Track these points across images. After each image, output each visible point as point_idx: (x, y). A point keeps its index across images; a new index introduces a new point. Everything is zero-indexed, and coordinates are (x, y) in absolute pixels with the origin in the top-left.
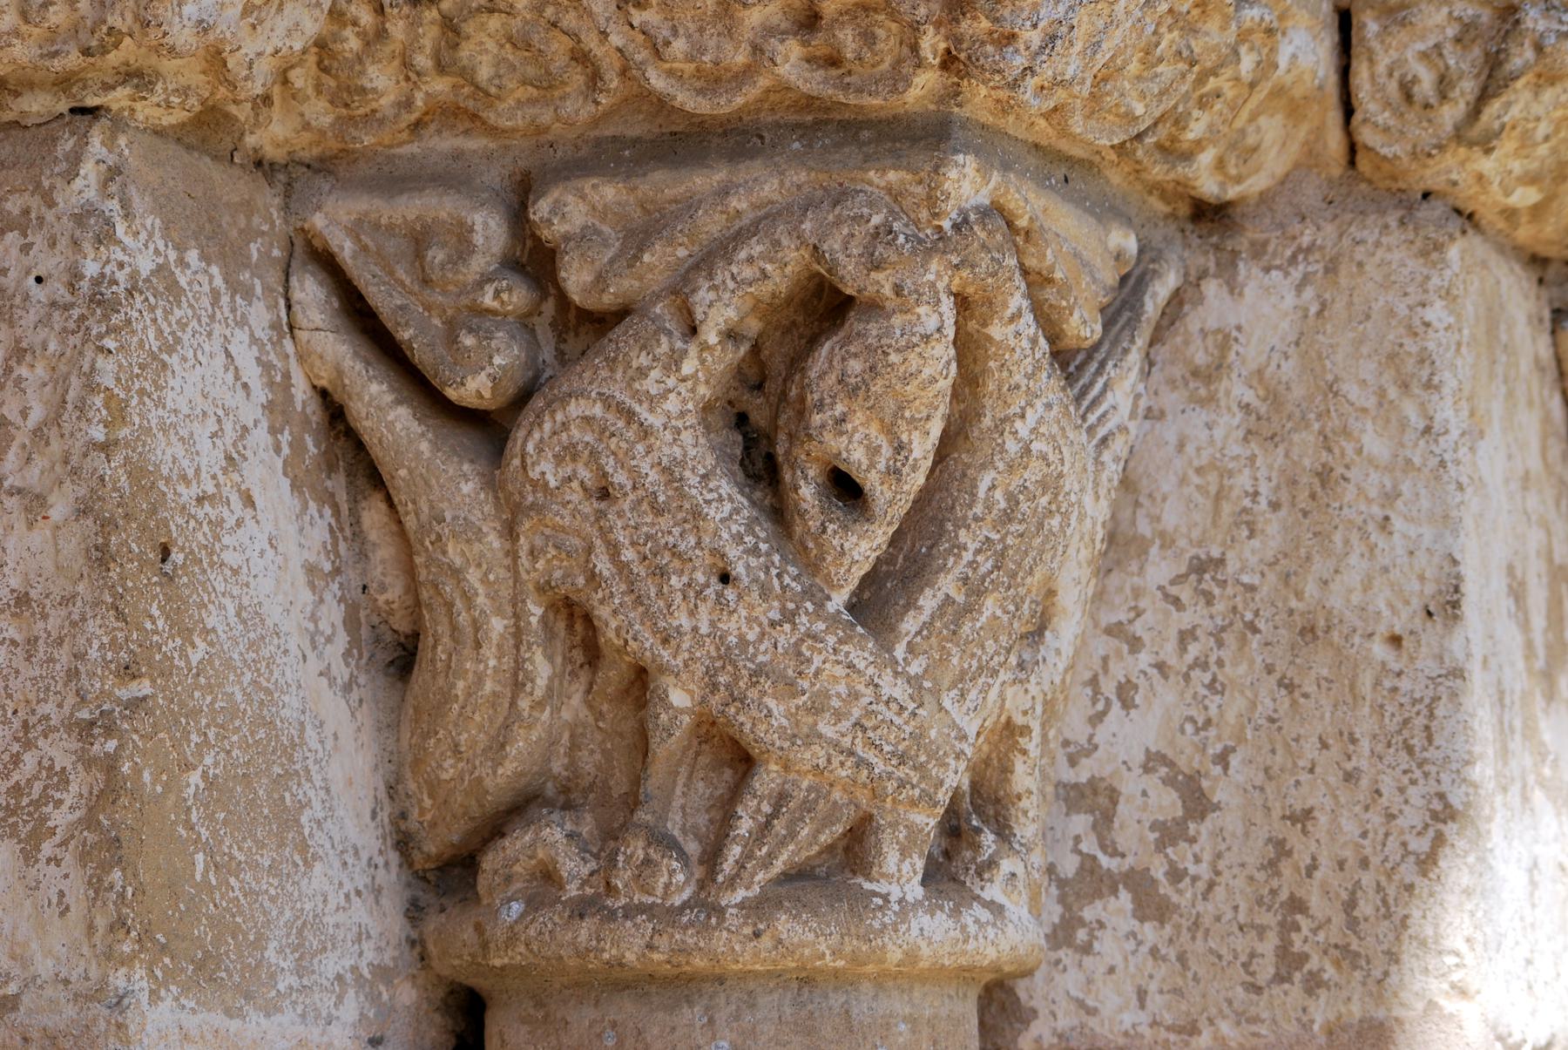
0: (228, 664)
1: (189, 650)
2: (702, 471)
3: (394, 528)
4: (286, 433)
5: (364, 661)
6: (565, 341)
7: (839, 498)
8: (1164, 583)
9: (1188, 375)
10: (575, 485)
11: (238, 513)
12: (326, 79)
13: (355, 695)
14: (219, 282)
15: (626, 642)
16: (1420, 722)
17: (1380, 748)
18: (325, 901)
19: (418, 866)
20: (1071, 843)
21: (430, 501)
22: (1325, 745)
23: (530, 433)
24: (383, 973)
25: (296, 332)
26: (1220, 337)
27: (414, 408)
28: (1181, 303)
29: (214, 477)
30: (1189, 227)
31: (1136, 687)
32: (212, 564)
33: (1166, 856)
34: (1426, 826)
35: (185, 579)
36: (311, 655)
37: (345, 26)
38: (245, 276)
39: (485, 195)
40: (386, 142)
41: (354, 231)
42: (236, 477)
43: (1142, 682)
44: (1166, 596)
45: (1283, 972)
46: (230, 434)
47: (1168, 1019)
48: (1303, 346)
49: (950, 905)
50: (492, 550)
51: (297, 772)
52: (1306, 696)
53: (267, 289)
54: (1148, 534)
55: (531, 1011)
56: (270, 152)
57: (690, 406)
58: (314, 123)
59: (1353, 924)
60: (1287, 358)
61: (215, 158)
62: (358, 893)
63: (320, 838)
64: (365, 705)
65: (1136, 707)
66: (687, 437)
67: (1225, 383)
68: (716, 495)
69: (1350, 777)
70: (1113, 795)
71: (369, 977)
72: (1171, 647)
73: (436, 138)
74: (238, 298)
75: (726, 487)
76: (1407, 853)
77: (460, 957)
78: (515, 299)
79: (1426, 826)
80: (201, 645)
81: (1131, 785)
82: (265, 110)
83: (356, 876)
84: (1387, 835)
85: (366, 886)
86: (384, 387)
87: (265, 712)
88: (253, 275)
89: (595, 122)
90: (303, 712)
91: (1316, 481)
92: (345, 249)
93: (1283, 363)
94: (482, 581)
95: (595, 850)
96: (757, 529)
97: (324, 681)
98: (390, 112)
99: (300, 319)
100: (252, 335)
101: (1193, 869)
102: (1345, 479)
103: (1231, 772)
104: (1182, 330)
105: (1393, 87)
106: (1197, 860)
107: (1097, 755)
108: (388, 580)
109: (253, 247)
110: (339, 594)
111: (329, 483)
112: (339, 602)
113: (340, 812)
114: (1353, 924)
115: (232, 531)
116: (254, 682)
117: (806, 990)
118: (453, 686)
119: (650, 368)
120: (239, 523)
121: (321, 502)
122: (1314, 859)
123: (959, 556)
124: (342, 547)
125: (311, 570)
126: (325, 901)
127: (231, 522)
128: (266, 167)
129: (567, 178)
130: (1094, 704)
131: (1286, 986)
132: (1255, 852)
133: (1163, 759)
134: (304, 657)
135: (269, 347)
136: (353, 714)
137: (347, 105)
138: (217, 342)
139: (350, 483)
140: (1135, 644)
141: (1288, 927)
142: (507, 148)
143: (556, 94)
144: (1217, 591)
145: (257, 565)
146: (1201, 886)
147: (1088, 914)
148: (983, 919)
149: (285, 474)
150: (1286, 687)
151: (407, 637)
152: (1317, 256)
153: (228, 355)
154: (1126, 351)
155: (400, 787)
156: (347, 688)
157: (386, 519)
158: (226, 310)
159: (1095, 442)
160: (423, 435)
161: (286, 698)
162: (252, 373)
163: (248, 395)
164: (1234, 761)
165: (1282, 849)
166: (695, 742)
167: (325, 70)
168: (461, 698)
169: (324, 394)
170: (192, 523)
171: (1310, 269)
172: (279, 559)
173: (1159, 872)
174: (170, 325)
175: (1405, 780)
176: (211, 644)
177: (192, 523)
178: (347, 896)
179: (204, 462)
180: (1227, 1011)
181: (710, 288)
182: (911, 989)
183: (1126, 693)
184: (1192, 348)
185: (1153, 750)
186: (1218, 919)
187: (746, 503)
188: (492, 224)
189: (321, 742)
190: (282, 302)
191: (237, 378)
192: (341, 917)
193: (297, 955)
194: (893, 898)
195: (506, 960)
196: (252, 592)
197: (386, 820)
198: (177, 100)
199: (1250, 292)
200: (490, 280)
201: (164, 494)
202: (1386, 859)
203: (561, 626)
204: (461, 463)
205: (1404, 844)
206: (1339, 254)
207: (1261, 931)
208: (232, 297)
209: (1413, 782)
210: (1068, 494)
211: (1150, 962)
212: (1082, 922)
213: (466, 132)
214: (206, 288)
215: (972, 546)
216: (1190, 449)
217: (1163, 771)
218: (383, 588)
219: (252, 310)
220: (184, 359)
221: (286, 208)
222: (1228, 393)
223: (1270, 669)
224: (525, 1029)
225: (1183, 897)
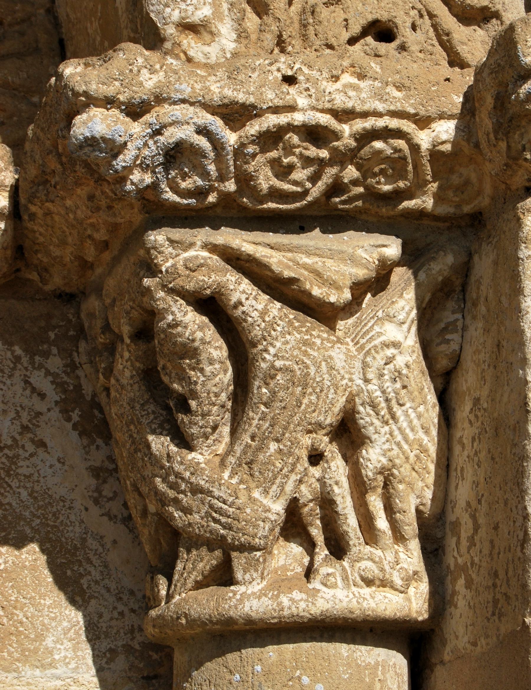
57: (134, 373)
78: (108, 337)
123: (250, 425)
215: (257, 417)
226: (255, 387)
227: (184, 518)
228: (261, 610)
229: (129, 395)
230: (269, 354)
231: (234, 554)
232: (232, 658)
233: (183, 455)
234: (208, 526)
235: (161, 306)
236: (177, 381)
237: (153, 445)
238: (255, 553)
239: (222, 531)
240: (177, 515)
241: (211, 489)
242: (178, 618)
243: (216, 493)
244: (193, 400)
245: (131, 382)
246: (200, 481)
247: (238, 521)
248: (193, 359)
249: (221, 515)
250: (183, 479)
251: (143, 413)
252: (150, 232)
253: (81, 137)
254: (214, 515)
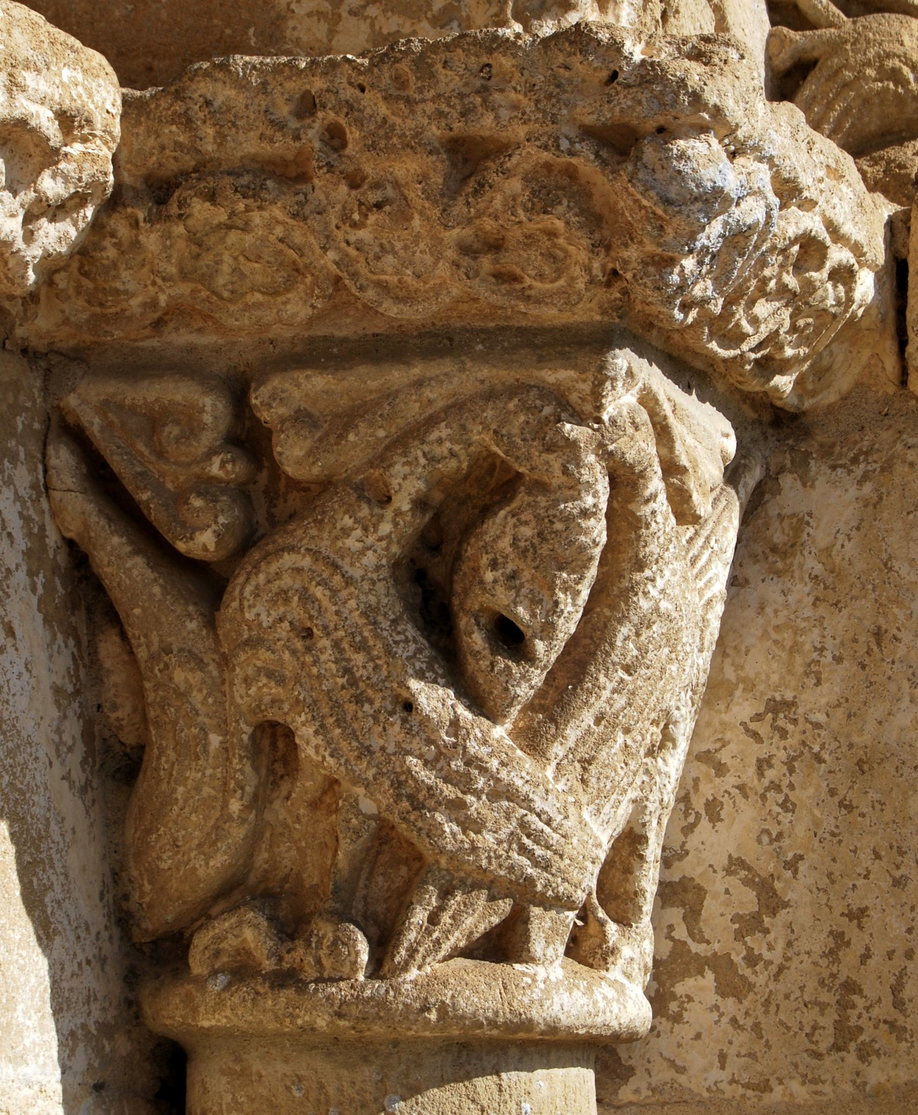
2: (392, 617)
3: (126, 657)
4: (41, 575)
5: (97, 767)
7: (504, 642)
9: (767, 551)
10: (286, 625)
12: (85, 282)
13: (89, 796)
15: (324, 758)
18: (62, 969)
19: (135, 940)
20: (665, 931)
21: (160, 636)
22: (877, 856)
23: (248, 580)
24: (106, 1030)
25: (51, 492)
26: (795, 520)
27: (148, 558)
28: (762, 494)
30: (770, 431)
31: (722, 804)
33: (745, 943)
36: (56, 763)
39: (213, 383)
40: (132, 336)
43: (726, 800)
44: (747, 730)
47: (745, 1078)
48: (863, 530)
49: (583, 984)
50: (211, 677)
51: (42, 861)
52: (863, 815)
53: (28, 455)
54: (734, 680)
55: (231, 1065)
57: (384, 562)
58: (73, 319)
59: (899, 1004)
60: (849, 540)
62: (89, 962)
64: (96, 805)
65: (722, 820)
66: (381, 587)
67: (799, 558)
68: (403, 637)
70: (701, 892)
71: (95, 1032)
72: (752, 771)
73: (174, 335)
81: (717, 884)
82: (32, 306)
83: (87, 948)
85: (94, 956)
86: (124, 540)
87: (19, 809)
88: (18, 443)
90: (49, 810)
91: (872, 639)
92: (94, 424)
93: (846, 543)
94: (203, 704)
95: (290, 932)
96: (436, 666)
97: (66, 784)
98: (138, 311)
99: (55, 482)
100: (16, 493)
101: (767, 955)
102: (896, 639)
103: (799, 876)
104: (763, 515)
106: (770, 948)
107: (687, 859)
110: (79, 711)
111: (73, 619)
112: (79, 718)
116: (11, 784)
118: (174, 791)
121: (66, 635)
122: (868, 949)
123: (599, 697)
125: (57, 690)
126: (62, 969)
128: (31, 354)
129: (285, 370)
130: (686, 817)
131: (844, 1054)
134: (51, 763)
135: (29, 504)
136: (87, 813)
137: (101, 305)
140: (721, 769)
141: (844, 1005)
142: (234, 343)
146: (773, 969)
147: (680, 989)
148: (610, 996)
149: (39, 610)
150: (846, 807)
151: (132, 748)
154: (726, 529)
155: (124, 874)
159: (703, 602)
160: (155, 580)
161: (35, 798)
163: (12, 543)
165: (839, 939)
166: (377, 844)
167: (86, 275)
168: (181, 802)
169: (70, 544)
171: (869, 468)
172: (33, 681)
173: (737, 958)
178: (80, 965)
180: (794, 1074)
181: (404, 464)
182: (549, 1052)
183: (713, 809)
185: (735, 856)
186: (787, 997)
188: (220, 406)
189: (62, 835)
190: (40, 467)
192: (75, 983)
193: (40, 1014)
195: (213, 1023)
196: (11, 708)
197: (111, 901)
199: (821, 483)
200: (216, 453)
203: (266, 743)
204: (187, 604)
206: (893, 457)
207: (823, 1007)
210: (684, 644)
212: (674, 997)
215: (610, 686)
216: (769, 610)
217: (743, 873)
218: (115, 707)
219: (17, 472)
221: (45, 389)
223: (832, 792)
224: (224, 1080)
225: (760, 978)
226: (620, 637)
227: (460, 837)
230: (654, 586)
231: (536, 911)
233: (485, 728)
234: (509, 857)
235: (585, 478)
236: (526, 602)
238: (567, 913)
239: (530, 871)
240: (448, 830)
241: (531, 796)
242: (425, 1008)
243: (538, 805)
244: (541, 639)
246: (515, 779)
247: (561, 856)
250: (484, 770)
251: (398, 638)
253: (709, 185)
254: (525, 840)
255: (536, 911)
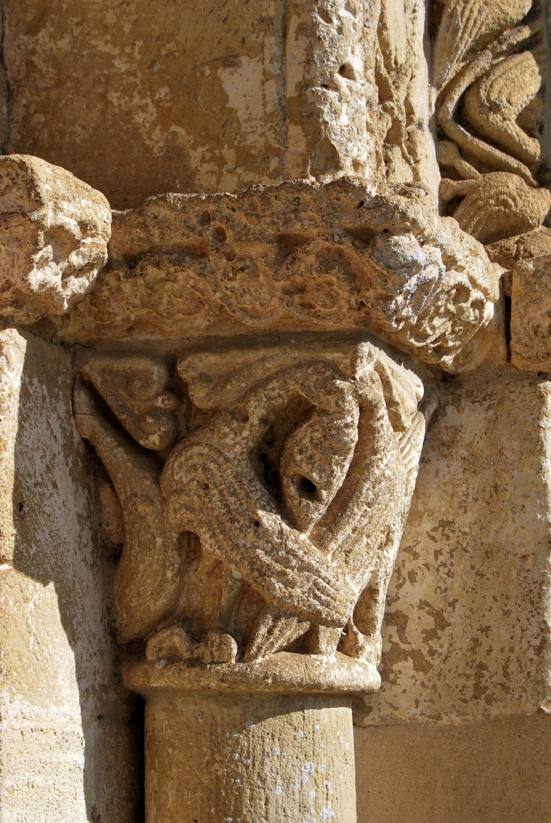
0: (45, 556)
1: (30, 549)
2: (249, 478)
4: (71, 457)
5: (99, 555)
6: (190, 422)
8: (429, 531)
11: (51, 491)
13: (95, 569)
14: (45, 392)
15: (214, 550)
16: (536, 591)
17: (519, 601)
18: (82, 657)
21: (131, 488)
22: (496, 600)
23: (176, 459)
25: (76, 415)
26: (453, 429)
28: (437, 416)
29: (41, 475)
30: (441, 384)
31: (416, 573)
32: (40, 512)
33: (428, 644)
34: (538, 635)
35: (29, 518)
36: (79, 552)
37: (103, 286)
38: (56, 390)
39: (158, 359)
41: (103, 372)
42: (50, 475)
43: (418, 571)
44: (429, 536)
45: (477, 694)
46: (48, 457)
47: (428, 712)
48: (488, 434)
49: (346, 665)
51: (71, 602)
53: (64, 396)
55: (167, 706)
56: (68, 339)
57: (245, 450)
58: (87, 327)
59: (506, 675)
61: (45, 340)
62: (95, 654)
63: (80, 630)
67: (455, 449)
69: (506, 613)
71: (98, 689)
74: (53, 400)
75: (259, 486)
76: (530, 646)
77: (138, 682)
78: (170, 403)
79: (538, 635)
80: (34, 547)
81: (414, 614)
84: (522, 638)
86: (113, 439)
88: (59, 390)
89: (208, 328)
91: (493, 490)
92: (98, 381)
93: (480, 441)
97: (83, 563)
98: (120, 323)
99: (78, 410)
100: (58, 415)
101: (439, 650)
104: (437, 426)
105: (530, 329)
106: (441, 646)
107: (399, 601)
108: (110, 521)
109: (60, 379)
111: (87, 479)
113: (88, 619)
114: (506, 675)
115: (48, 498)
116: (55, 563)
117: (286, 700)
118: (138, 567)
119: (229, 434)
120: (51, 495)
122: (491, 647)
123: (354, 519)
124: (92, 507)
125: (79, 516)
126: (82, 657)
127: (48, 494)
129: (195, 353)
130: (398, 580)
131: (479, 700)
132: (464, 643)
133: (427, 604)
134: (76, 553)
135: (65, 421)
137: (101, 320)
138: (44, 417)
139: (96, 480)
140: (416, 556)
141: (479, 676)
142: (169, 339)
143: (192, 317)
144: (451, 534)
145: (58, 513)
146: (443, 657)
147: (395, 667)
148: (360, 671)
149: (70, 475)
150: (479, 575)
152: (494, 397)
153: (49, 423)
154: (418, 434)
156: (92, 566)
157: (110, 495)
158: (48, 404)
159: (407, 471)
160: (129, 460)
161: (68, 570)
162: (58, 432)
163: (56, 441)
164: (457, 605)
165: (476, 642)
166: (241, 593)
167: (94, 304)
169: (86, 441)
170: (32, 495)
171: (491, 403)
173: (424, 652)
174: (25, 409)
175: (530, 615)
176: (38, 547)
177: (32, 495)
178: (90, 655)
179: (38, 468)
181: (255, 401)
183: (412, 576)
184: (442, 434)
185: (423, 600)
186: (450, 671)
187: (267, 492)
188: (162, 371)
189: (82, 589)
190: (70, 402)
191: (52, 433)
192: (88, 664)
194: (324, 662)
195: (158, 684)
196: (55, 525)
197: (106, 623)
198: (32, 314)
199: (467, 411)
201: (21, 482)
202: (521, 648)
204: (145, 472)
205: (529, 642)
206: (503, 397)
207: (468, 677)
208: (51, 399)
209: (533, 616)
211: (421, 688)
212: (392, 671)
213: (152, 333)
214: (40, 395)
215: (360, 513)
216: (440, 475)
217: (427, 609)
218: (108, 524)
219: (58, 405)
220: (31, 424)
221: (73, 362)
222: (457, 453)
223: (473, 567)
227: (284, 590)
228: (341, 679)
229: (234, 469)
231: (322, 628)
232: (296, 716)
233: (296, 535)
234: (308, 600)
235: (347, 408)
237: (264, 520)
240: (277, 587)
242: (266, 677)
243: (323, 574)
244: (325, 490)
245: (240, 458)
247: (335, 600)
248: (341, 456)
249: (323, 593)
250: (296, 556)
252: (363, 343)
253: (410, 259)
255: (322, 628)
